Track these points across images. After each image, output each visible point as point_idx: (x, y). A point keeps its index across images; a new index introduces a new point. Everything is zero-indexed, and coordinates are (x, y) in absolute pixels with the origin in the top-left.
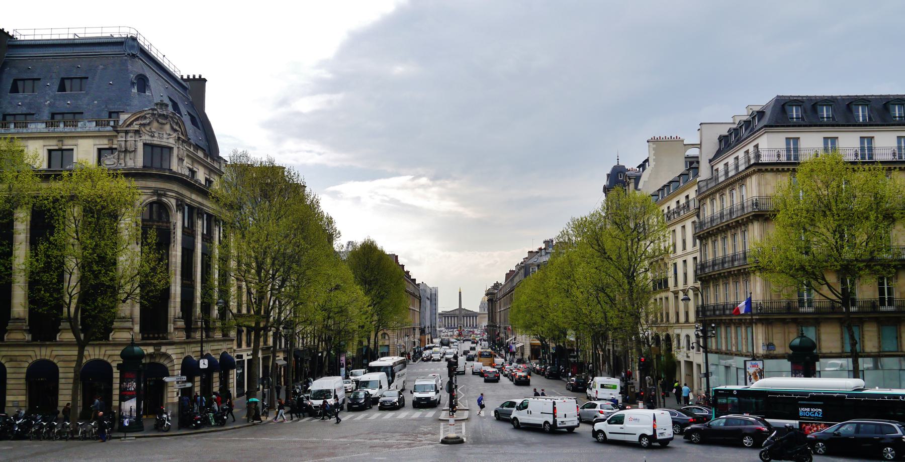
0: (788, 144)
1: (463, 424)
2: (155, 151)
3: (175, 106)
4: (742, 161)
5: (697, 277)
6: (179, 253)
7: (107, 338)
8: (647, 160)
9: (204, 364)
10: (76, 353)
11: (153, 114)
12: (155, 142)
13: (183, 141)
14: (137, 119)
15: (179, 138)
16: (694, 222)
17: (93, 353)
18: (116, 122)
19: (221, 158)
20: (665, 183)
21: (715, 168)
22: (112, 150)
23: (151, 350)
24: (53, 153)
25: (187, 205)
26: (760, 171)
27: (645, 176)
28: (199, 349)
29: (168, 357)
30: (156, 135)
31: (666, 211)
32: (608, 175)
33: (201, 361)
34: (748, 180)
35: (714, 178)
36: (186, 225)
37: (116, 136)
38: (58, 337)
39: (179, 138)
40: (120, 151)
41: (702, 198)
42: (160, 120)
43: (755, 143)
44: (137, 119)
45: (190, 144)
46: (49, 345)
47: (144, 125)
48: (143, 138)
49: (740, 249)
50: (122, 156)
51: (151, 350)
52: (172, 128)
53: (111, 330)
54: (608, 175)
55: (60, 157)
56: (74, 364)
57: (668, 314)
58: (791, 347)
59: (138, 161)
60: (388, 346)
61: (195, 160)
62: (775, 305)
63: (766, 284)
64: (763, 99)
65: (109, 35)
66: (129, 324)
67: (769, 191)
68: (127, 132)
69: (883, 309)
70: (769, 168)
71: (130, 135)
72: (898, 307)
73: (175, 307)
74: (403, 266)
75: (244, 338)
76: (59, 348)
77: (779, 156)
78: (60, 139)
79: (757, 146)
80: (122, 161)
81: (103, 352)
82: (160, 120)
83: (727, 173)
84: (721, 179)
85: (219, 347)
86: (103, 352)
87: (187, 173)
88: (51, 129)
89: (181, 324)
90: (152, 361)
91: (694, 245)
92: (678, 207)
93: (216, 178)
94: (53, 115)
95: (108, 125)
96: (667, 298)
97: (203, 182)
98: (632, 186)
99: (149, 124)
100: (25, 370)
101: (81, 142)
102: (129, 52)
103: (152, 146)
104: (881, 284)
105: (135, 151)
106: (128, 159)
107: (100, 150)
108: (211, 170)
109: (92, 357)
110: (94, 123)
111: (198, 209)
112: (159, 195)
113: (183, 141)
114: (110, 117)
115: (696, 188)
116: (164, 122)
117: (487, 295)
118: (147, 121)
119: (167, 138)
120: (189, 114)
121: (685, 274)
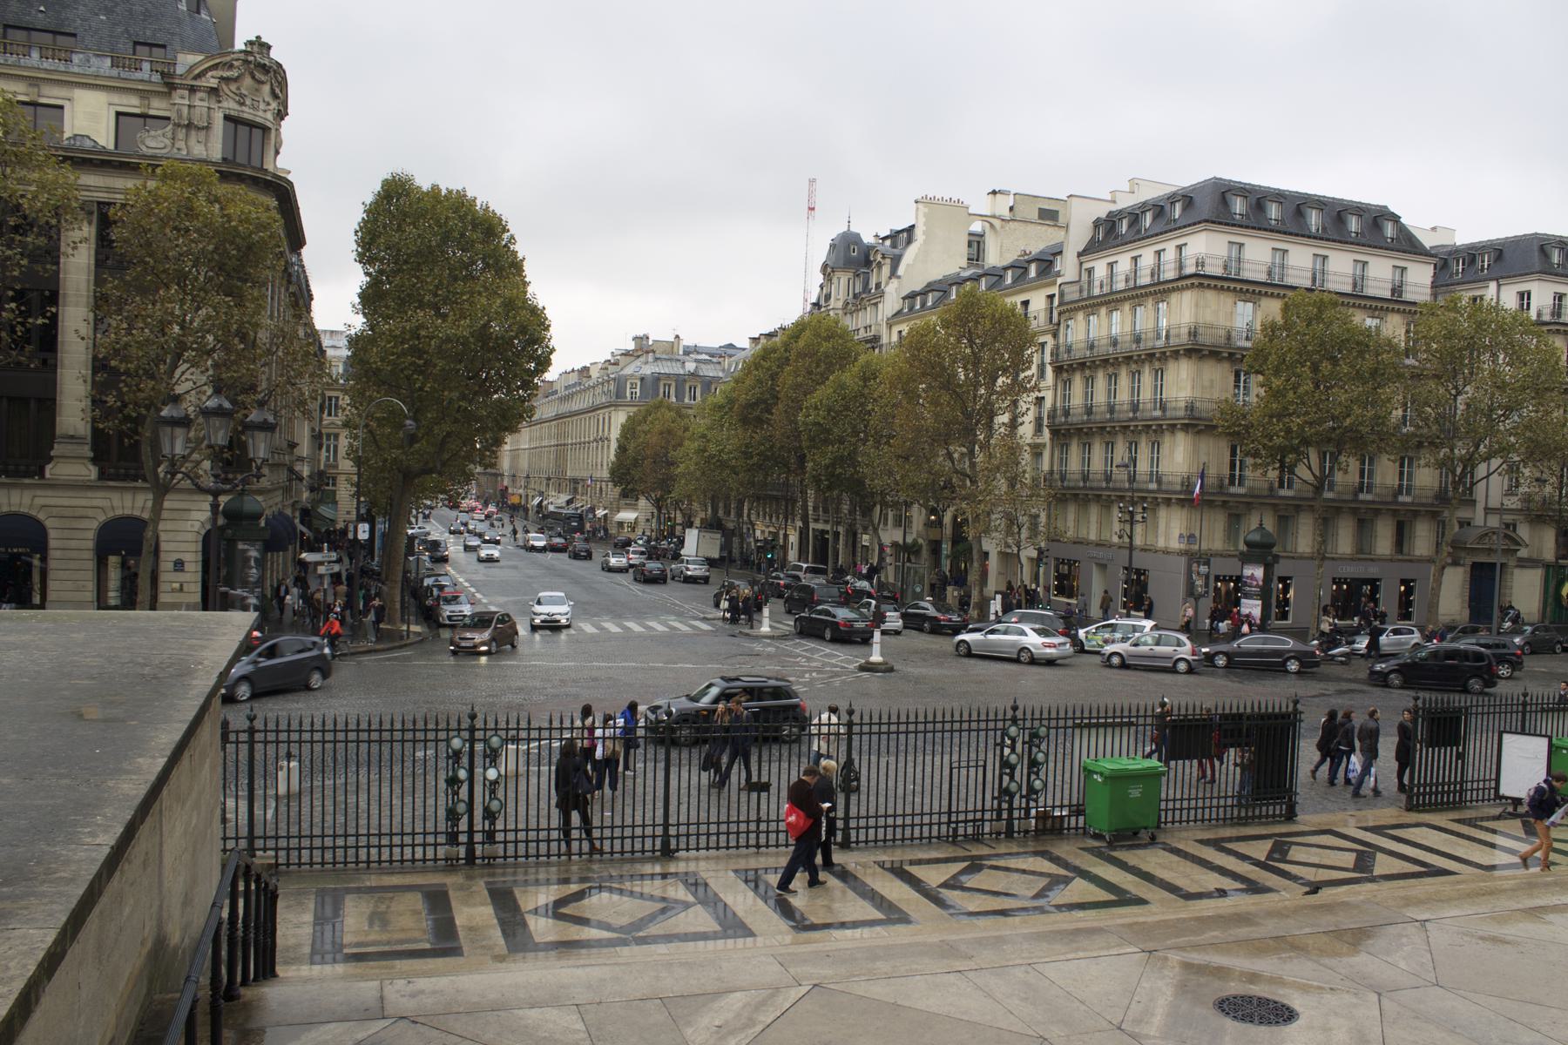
7: (42, 474)
11: (246, 62)
12: (246, 116)
21: (1086, 266)
26: (1201, 285)
30: (248, 102)
34: (1174, 298)
38: (49, 470)
40: (179, 125)
42: (258, 75)
46: (28, 486)
48: (224, 104)
67: (1208, 317)
69: (1233, 490)
70: (1213, 283)
71: (199, 95)
72: (1251, 488)
76: (49, 493)
80: (181, 144)
82: (258, 75)
98: (886, 270)
99: (236, 80)
100: (91, 535)
101: (79, 93)
104: (1402, 466)
105: (207, 128)
109: (119, 512)
110: (108, 62)
116: (263, 78)
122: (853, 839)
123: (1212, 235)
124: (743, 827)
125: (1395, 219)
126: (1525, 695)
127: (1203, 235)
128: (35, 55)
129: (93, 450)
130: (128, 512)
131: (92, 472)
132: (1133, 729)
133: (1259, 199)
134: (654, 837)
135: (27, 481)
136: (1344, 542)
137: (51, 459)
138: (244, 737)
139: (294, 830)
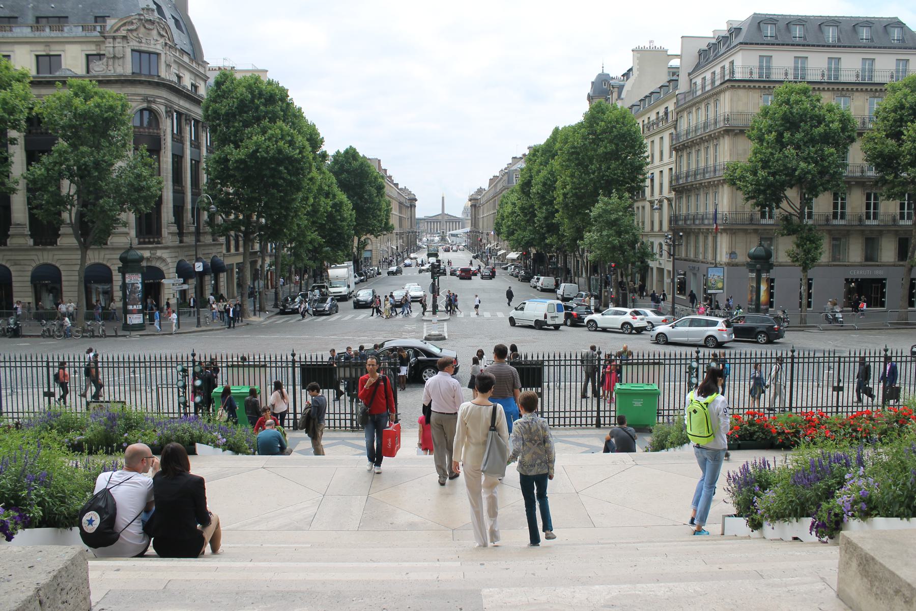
0: (761, 62)
1: (445, 323)
4: (718, 77)
5: (673, 188)
6: (170, 160)
7: (5, 244)
8: (631, 70)
9: (199, 267)
10: (80, 257)
12: (143, 49)
13: (170, 47)
14: (124, 24)
15: (166, 44)
16: (671, 134)
17: (95, 257)
18: (103, 27)
20: (647, 93)
21: (693, 81)
22: (100, 56)
25: (176, 111)
26: (733, 87)
27: (628, 85)
28: (194, 253)
29: (163, 260)
30: (144, 41)
31: (646, 122)
32: (593, 83)
34: (722, 96)
35: (692, 91)
36: (175, 132)
37: (104, 42)
39: (166, 44)
41: (681, 110)
43: (730, 59)
44: (124, 24)
47: (131, 31)
48: (131, 44)
49: (711, 162)
52: (159, 33)
54: (593, 83)
55: (48, 61)
56: (78, 268)
58: (750, 256)
59: (126, 68)
61: (181, 65)
62: (739, 216)
63: (733, 199)
64: (742, 14)
67: (741, 108)
68: (114, 38)
70: (742, 84)
71: (118, 40)
73: (167, 213)
74: (385, 170)
76: (60, 253)
77: (751, 73)
79: (732, 63)
80: (111, 68)
82: (147, 26)
83: (703, 87)
84: (699, 93)
85: (210, 251)
86: (102, 256)
87: (175, 79)
88: (37, 33)
89: (174, 229)
91: (671, 157)
92: (657, 118)
93: (202, 83)
94: (38, 19)
95: (95, 30)
96: (643, 207)
98: (615, 95)
99: (136, 30)
100: (29, 274)
101: (69, 47)
105: (123, 57)
106: (116, 66)
107: (88, 56)
108: (197, 75)
110: (81, 28)
111: (186, 115)
112: (149, 102)
113: (170, 47)
114: (96, 22)
115: (674, 100)
116: (151, 27)
117: (470, 200)
118: (134, 27)
121: (661, 185)
122: (602, 422)
123: (746, 52)
124: (573, 414)
125: (900, 25)
126: (886, 350)
127: (740, 54)
129: (30, 230)
130: (97, 261)
131: (31, 242)
132: (662, 367)
133: (790, 22)
134: (592, 417)
135: (49, 247)
136: (855, 252)
137: (8, 236)
138: (789, 360)
139: (804, 405)
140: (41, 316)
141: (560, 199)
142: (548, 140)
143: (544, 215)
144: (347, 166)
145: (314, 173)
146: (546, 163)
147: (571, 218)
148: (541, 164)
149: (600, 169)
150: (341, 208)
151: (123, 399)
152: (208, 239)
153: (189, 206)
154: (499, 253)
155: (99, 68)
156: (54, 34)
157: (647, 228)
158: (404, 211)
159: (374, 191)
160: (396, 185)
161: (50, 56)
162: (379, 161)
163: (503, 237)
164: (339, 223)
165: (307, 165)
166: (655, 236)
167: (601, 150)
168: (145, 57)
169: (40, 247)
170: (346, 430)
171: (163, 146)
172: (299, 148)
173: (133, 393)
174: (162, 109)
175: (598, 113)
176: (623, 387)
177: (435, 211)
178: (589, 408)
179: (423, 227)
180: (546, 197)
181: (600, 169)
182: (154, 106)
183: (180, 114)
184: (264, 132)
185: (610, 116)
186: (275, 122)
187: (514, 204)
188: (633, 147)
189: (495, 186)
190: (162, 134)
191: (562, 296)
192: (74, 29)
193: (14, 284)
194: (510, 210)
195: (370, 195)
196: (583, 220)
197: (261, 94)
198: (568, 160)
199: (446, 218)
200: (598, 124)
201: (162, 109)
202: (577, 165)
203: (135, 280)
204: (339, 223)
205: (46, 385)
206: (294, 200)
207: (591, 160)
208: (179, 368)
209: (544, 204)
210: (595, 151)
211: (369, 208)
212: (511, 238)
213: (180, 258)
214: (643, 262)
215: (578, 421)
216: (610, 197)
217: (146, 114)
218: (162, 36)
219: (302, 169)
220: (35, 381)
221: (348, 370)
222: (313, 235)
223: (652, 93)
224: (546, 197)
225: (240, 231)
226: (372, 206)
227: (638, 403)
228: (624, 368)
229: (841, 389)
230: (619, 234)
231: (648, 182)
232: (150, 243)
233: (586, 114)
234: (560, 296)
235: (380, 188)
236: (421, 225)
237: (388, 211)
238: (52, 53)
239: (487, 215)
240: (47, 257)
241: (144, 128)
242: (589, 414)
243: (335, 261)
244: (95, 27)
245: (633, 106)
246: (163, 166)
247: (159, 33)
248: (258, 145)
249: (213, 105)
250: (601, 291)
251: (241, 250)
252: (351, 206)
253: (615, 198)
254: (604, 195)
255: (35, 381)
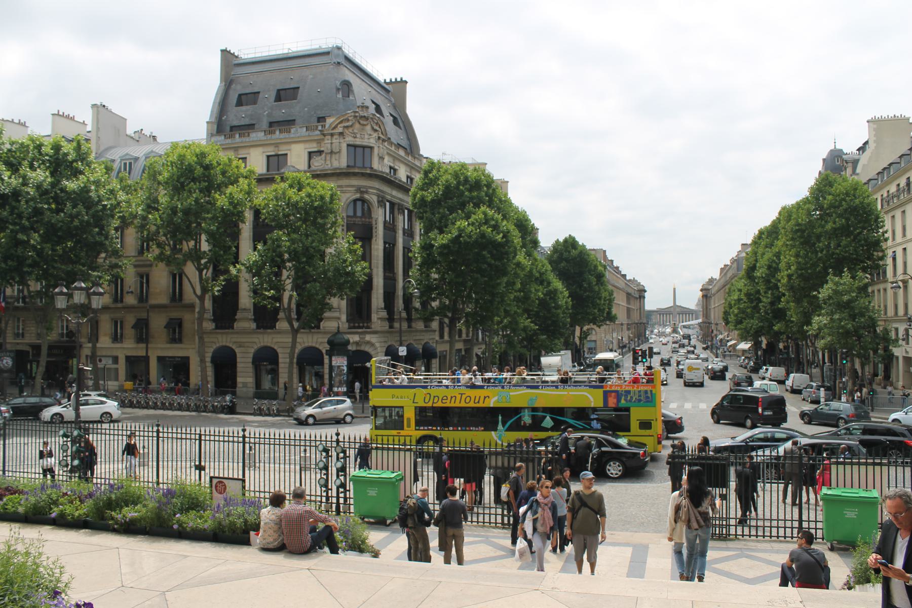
2: (359, 151)
3: (378, 109)
7: (233, 328)
8: (866, 143)
10: (290, 340)
11: (355, 117)
12: (358, 143)
14: (341, 122)
15: (379, 138)
19: (422, 156)
20: (886, 166)
22: (320, 152)
23: (356, 338)
24: (271, 158)
27: (864, 159)
31: (885, 195)
32: (824, 160)
33: (401, 349)
36: (388, 218)
37: (323, 140)
39: (379, 138)
42: (362, 122)
44: (341, 122)
45: (391, 143)
46: (270, 333)
47: (347, 127)
48: (347, 139)
50: (328, 158)
51: (356, 338)
52: (373, 128)
53: (321, 320)
54: (824, 160)
55: (276, 161)
57: (886, 307)
59: (342, 162)
60: (595, 341)
61: (395, 158)
65: (317, 47)
66: (336, 314)
68: (332, 135)
75: (446, 330)
76: (279, 336)
78: (276, 145)
80: (328, 162)
81: (315, 340)
82: (362, 122)
86: (315, 340)
88: (269, 136)
89: (384, 314)
90: (359, 348)
92: (898, 190)
94: (271, 124)
96: (885, 290)
97: (404, 180)
98: (849, 170)
99: (351, 126)
100: (251, 355)
102: (335, 61)
103: (355, 146)
105: (339, 152)
106: (333, 160)
107: (310, 153)
108: (412, 167)
109: (306, 345)
111: (399, 204)
112: (362, 192)
114: (319, 122)
118: (350, 123)
119: (370, 139)
120: (391, 115)
128: (278, 132)
130: (310, 344)
131: (253, 325)
137: (235, 320)
140: (260, 394)
141: (785, 281)
142: (774, 222)
143: (769, 300)
144: (565, 255)
145: (521, 257)
146: (771, 245)
147: (798, 301)
148: (766, 247)
149: (828, 246)
150: (555, 295)
151: (241, 477)
152: (420, 325)
153: (400, 293)
154: (729, 344)
155: (319, 163)
156: (283, 135)
157: (891, 312)
158: (632, 302)
159: (593, 280)
160: (624, 276)
161: (278, 155)
162: (605, 252)
163: (731, 326)
164: (554, 310)
165: (511, 249)
166: (901, 321)
167: (829, 226)
168: (359, 150)
169: (262, 330)
170: (496, 527)
171: (374, 234)
172: (502, 232)
173: (142, 468)
174: (374, 199)
175: (825, 186)
176: (829, 492)
177: (667, 303)
178: (788, 517)
179: (655, 319)
180: (770, 281)
181: (828, 246)
182: (366, 196)
183: (392, 205)
184: (468, 217)
185: (838, 188)
186: (479, 208)
187: (740, 290)
188: (867, 221)
189: (725, 274)
190: (374, 223)
191: (792, 387)
192: (299, 130)
193: (238, 365)
194: (736, 297)
195: (590, 284)
196: (811, 303)
197: (466, 180)
198: (793, 239)
199: (678, 310)
200: (825, 198)
201: (374, 199)
202: (802, 243)
203: (340, 362)
204: (554, 310)
205: (197, 459)
206: (499, 284)
207: (818, 238)
208: (321, 448)
209: (769, 289)
210: (823, 227)
211: (588, 297)
212: (739, 326)
213: (389, 343)
214: (886, 349)
215: (774, 533)
216: (841, 277)
217: (359, 204)
218: (376, 131)
219: (507, 253)
220: (231, 456)
221: (500, 458)
222: (525, 322)
223: (890, 164)
224: (770, 281)
225: (447, 316)
226: (591, 295)
227: (851, 514)
228: (834, 467)
229: (203, 468)
230: (853, 317)
231: (889, 261)
232: (359, 327)
233: (812, 188)
234: (789, 388)
235: (600, 277)
236: (653, 317)
237: (610, 301)
238: (280, 153)
239: (718, 305)
240: (266, 339)
241: (357, 217)
242: (789, 524)
243: (550, 351)
244: (317, 127)
245: (870, 180)
246: (374, 253)
247: (373, 128)
248: (461, 231)
249: (420, 193)
250: (835, 382)
251: (446, 337)
252: (566, 294)
253: (846, 277)
254: (835, 275)
255: (231, 456)
